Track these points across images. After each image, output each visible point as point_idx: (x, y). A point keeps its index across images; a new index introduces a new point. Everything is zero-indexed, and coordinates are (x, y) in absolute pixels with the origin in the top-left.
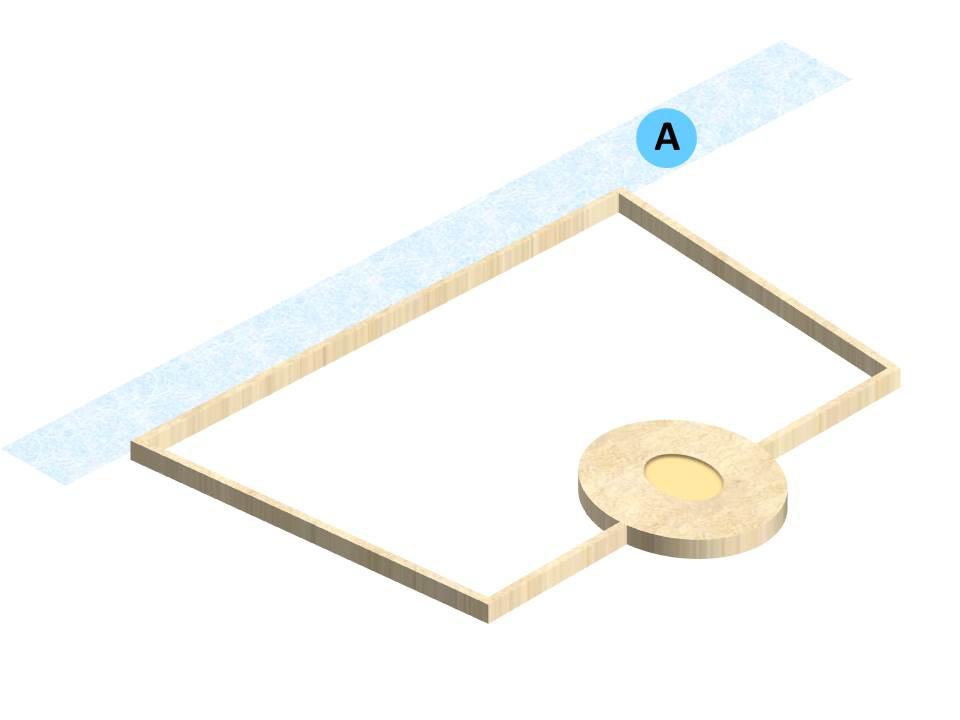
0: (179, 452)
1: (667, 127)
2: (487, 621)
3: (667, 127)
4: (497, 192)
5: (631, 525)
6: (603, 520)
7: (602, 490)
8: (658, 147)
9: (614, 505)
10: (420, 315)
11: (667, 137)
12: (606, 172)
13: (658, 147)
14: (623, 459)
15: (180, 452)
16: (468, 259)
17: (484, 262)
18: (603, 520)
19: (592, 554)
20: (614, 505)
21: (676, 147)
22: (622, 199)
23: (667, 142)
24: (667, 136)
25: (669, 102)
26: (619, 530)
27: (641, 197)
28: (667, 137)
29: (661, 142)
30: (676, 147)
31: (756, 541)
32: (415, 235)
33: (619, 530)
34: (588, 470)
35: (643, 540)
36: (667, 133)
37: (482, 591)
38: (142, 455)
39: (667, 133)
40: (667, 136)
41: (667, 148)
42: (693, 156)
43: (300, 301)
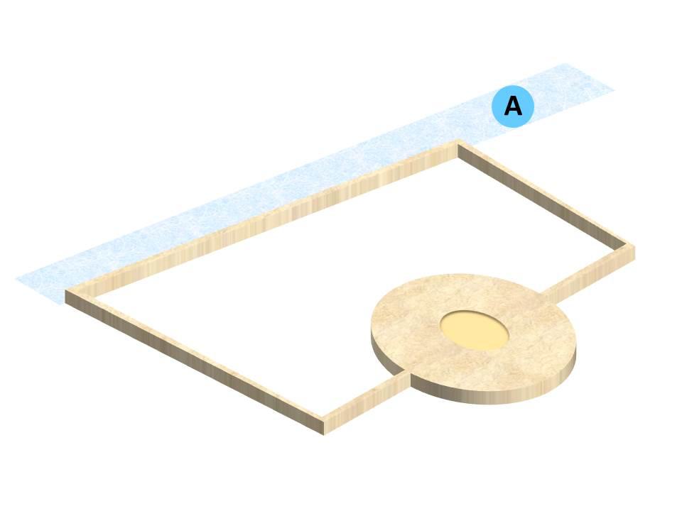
0: (103, 301)
1: (513, 98)
2: (323, 434)
3: (513, 98)
4: (365, 143)
5: (413, 373)
6: (394, 369)
7: (541, 338)
8: (507, 113)
9: (550, 349)
10: (118, 287)
11: (513, 106)
12: (442, 136)
13: (507, 113)
14: (556, 316)
15: (107, 301)
16: (426, 148)
17: (400, 165)
18: (394, 369)
19: (390, 391)
20: (550, 349)
21: (520, 113)
22: (461, 148)
23: (513, 109)
24: (513, 105)
25: (521, 81)
26: (405, 377)
27: (482, 149)
28: (513, 106)
29: (509, 109)
30: (520, 113)
31: (543, 387)
32: (307, 166)
33: (405, 377)
34: (531, 323)
35: (420, 384)
36: (513, 103)
37: (318, 412)
38: (73, 300)
39: (513, 103)
40: (513, 105)
41: (513, 113)
42: (530, 121)
43: (225, 201)
